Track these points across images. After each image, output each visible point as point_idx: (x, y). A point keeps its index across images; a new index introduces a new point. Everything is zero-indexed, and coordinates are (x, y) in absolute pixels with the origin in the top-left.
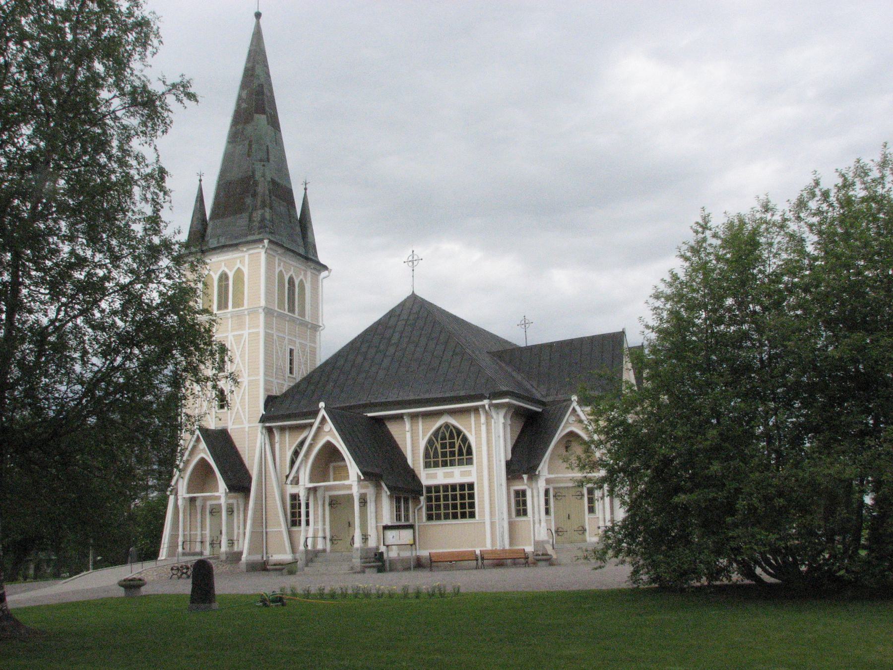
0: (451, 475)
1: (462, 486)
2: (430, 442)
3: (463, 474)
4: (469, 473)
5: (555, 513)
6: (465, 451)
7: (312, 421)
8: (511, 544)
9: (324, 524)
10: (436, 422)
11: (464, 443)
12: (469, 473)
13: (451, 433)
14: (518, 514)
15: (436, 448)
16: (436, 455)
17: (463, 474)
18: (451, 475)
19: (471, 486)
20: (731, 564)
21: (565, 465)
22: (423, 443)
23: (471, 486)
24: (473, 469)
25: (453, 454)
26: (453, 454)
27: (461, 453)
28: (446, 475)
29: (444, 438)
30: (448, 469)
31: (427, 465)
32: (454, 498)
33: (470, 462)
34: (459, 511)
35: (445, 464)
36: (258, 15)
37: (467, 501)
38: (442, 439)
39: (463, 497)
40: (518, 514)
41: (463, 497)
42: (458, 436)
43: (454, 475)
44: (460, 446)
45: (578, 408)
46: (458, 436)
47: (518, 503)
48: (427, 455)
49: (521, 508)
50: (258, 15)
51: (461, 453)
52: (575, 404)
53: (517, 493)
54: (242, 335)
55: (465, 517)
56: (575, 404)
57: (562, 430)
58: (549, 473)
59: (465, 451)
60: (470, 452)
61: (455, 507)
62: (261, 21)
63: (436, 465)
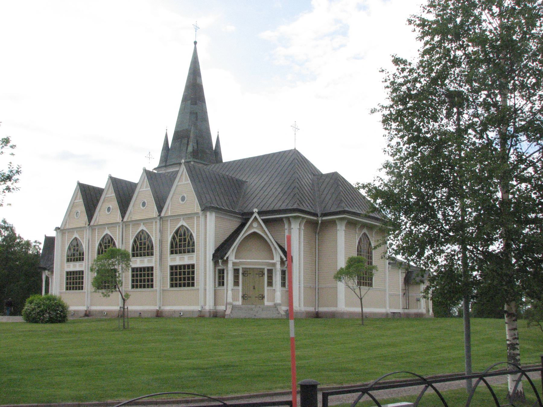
4: (81, 266)
5: (243, 283)
8: (215, 304)
10: (336, 247)
11: (191, 240)
14: (219, 285)
17: (180, 259)
20: (533, 36)
21: (70, 255)
28: (142, 261)
29: (181, 236)
30: (142, 258)
36: (195, 43)
40: (219, 285)
45: (258, 217)
48: (172, 247)
50: (195, 43)
52: (255, 215)
54: (255, 217)
56: (255, 215)
57: (246, 232)
58: (235, 259)
62: (197, 45)
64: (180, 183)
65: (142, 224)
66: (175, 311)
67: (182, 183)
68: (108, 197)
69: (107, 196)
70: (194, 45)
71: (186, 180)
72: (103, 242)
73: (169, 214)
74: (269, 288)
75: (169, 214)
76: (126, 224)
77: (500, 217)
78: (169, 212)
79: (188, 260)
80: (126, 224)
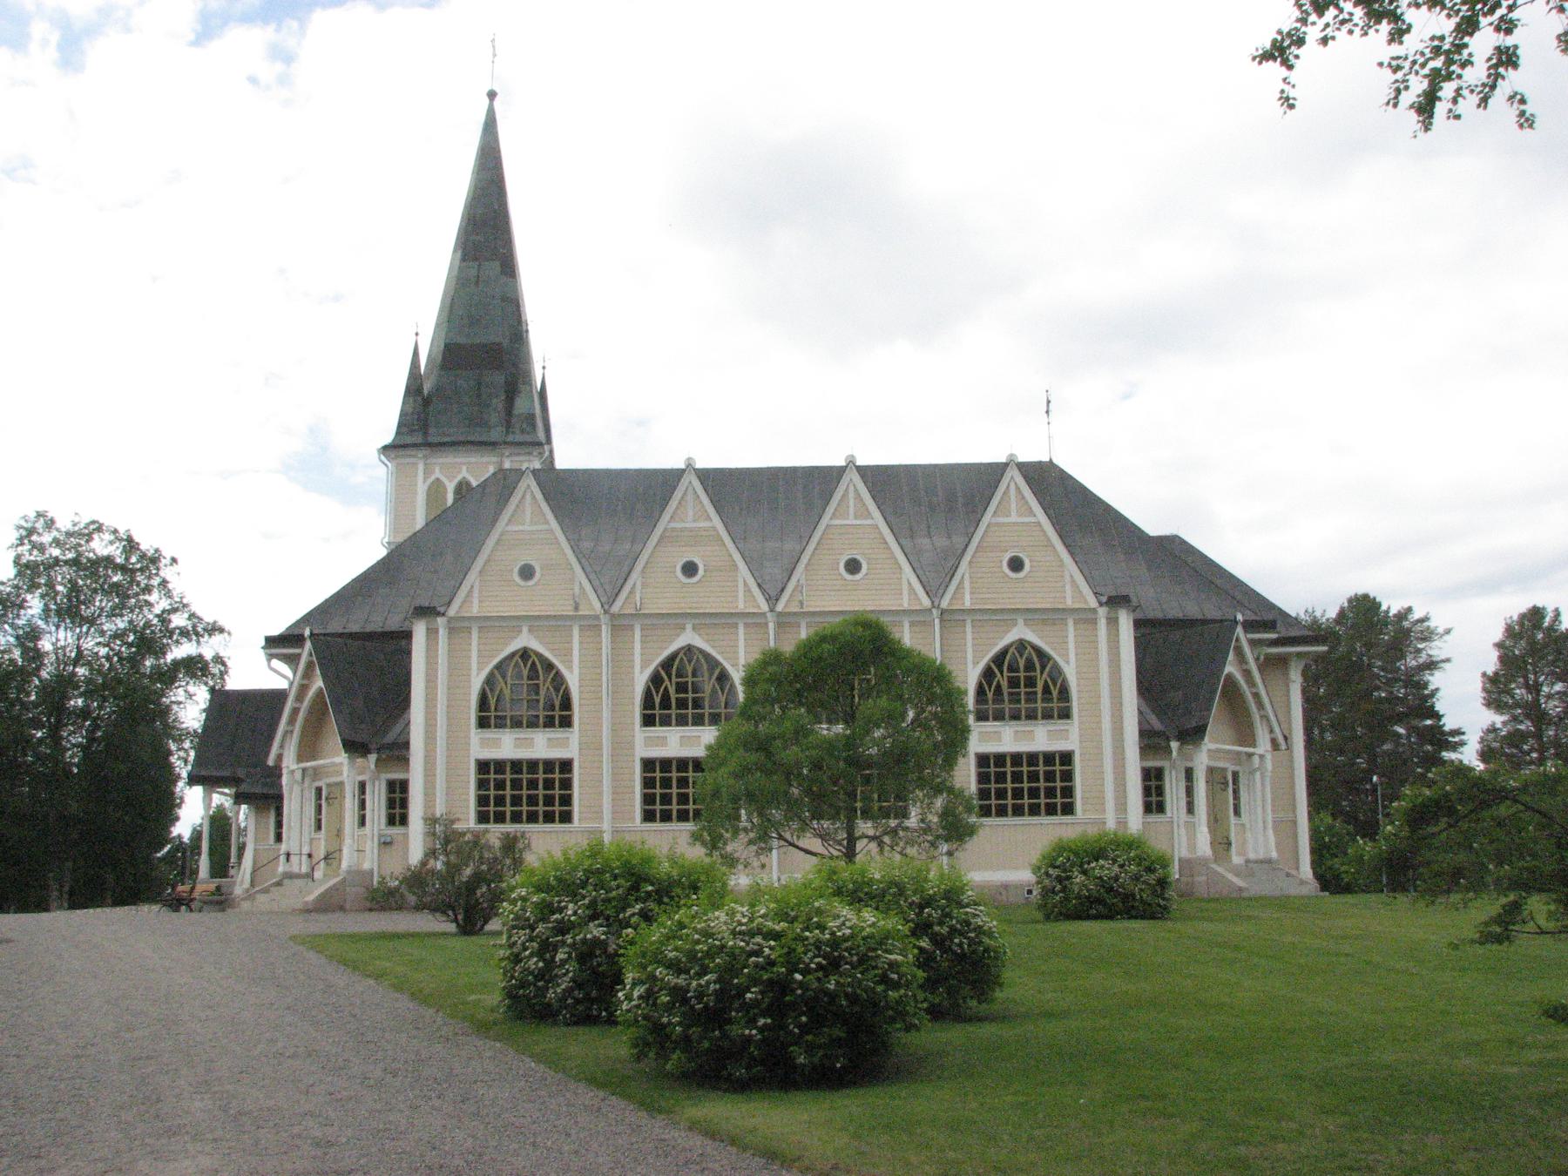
0: (663, 741)
2: (656, 680)
4: (564, 743)
7: (297, 651)
11: (557, 690)
12: (564, 743)
15: (999, 686)
16: (665, 703)
17: (519, 743)
18: (663, 741)
19: (1067, 758)
22: (641, 679)
23: (1067, 758)
32: (533, 784)
33: (1065, 714)
34: (1010, 802)
35: (682, 721)
36: (492, 95)
37: (1059, 784)
38: (1010, 669)
42: (711, 670)
44: (714, 691)
46: (1043, 668)
48: (648, 702)
50: (492, 95)
53: (391, 785)
55: (553, 821)
59: (657, 700)
62: (496, 103)
64: (509, 528)
65: (525, 629)
66: (1006, 886)
67: (1006, 520)
68: (673, 530)
69: (672, 525)
70: (487, 101)
71: (864, 513)
72: (1000, 667)
73: (968, 604)
74: (358, 832)
75: (475, 610)
76: (621, 626)
77: (849, 718)
78: (967, 596)
79: (516, 746)
80: (621, 626)
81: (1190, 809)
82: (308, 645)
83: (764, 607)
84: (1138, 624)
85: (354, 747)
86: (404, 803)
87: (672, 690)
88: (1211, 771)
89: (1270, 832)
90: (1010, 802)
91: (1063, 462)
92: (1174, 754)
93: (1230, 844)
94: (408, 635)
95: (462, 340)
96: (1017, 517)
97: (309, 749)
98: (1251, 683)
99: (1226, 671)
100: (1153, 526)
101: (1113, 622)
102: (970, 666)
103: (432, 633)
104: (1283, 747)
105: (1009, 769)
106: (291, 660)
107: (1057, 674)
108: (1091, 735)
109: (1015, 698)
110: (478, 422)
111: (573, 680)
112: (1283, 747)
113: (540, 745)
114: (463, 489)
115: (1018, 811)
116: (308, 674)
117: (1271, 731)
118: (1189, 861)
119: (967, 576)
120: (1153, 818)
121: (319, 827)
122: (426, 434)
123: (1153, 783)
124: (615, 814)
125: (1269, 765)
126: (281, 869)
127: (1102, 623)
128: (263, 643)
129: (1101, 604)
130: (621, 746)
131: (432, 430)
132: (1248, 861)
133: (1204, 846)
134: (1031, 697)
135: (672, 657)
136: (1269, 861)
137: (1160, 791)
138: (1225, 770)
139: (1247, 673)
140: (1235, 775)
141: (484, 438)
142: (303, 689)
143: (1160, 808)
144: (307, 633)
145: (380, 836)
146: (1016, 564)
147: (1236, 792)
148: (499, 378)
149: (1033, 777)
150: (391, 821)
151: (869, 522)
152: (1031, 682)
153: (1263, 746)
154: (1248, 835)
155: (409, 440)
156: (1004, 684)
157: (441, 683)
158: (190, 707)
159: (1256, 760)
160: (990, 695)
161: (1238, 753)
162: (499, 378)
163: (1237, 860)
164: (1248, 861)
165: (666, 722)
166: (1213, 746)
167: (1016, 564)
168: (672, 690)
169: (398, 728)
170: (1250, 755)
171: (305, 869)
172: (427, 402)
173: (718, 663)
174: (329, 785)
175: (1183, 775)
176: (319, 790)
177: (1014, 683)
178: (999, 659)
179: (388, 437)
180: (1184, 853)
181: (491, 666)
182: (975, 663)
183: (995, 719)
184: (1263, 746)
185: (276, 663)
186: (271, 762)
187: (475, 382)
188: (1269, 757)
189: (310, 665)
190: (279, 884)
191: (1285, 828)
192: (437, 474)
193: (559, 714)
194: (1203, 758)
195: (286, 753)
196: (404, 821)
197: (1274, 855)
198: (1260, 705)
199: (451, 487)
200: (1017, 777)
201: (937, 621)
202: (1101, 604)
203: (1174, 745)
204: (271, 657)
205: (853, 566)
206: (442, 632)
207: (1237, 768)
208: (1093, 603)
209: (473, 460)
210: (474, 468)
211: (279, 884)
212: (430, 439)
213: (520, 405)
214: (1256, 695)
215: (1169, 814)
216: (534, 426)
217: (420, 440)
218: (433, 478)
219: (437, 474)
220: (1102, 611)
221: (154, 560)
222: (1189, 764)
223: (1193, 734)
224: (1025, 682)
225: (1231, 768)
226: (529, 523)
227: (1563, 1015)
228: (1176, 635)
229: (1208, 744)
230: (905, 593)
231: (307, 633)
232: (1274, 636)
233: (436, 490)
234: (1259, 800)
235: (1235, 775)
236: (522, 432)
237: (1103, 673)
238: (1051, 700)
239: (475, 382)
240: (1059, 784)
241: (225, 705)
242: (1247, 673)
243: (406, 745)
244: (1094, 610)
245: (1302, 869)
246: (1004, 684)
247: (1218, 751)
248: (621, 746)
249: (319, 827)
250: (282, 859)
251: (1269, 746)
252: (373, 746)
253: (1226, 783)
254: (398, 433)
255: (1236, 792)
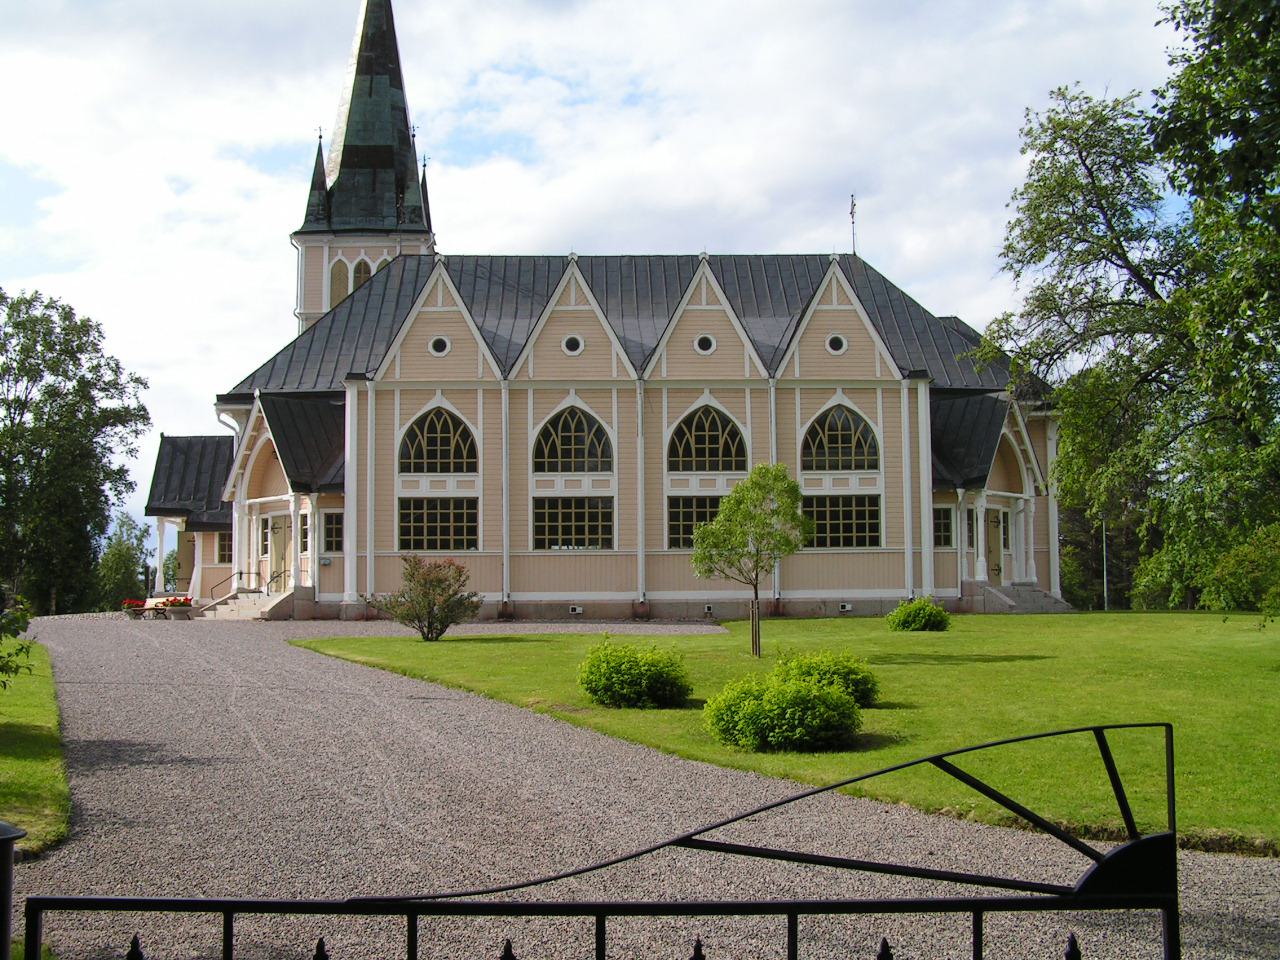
1: (459, 502)
3: (460, 484)
4: (873, 482)
6: (546, 452)
7: (248, 407)
9: (1027, 543)
12: (873, 482)
13: (713, 423)
15: (420, 444)
17: (460, 484)
19: (874, 500)
22: (533, 434)
24: (478, 478)
25: (579, 453)
26: (714, 453)
27: (727, 452)
29: (700, 427)
30: (841, 474)
31: (806, 466)
39: (861, 515)
41: (458, 518)
43: (852, 484)
44: (726, 442)
47: (329, 533)
48: (539, 452)
49: (334, 539)
51: (727, 452)
53: (329, 518)
59: (546, 452)
60: (607, 452)
61: (848, 528)
63: (419, 469)
78: (797, 369)
81: (971, 543)
82: (258, 403)
83: (634, 375)
84: (935, 393)
85: (301, 487)
86: (340, 533)
87: (558, 442)
88: (988, 511)
89: (1032, 562)
90: (828, 535)
91: (863, 255)
92: (960, 498)
93: (1000, 570)
94: (342, 395)
95: (358, 143)
96: (837, 302)
97: (259, 488)
98: (1021, 441)
99: (1002, 432)
100: (937, 311)
101: (913, 392)
102: (798, 426)
103: (362, 395)
104: (1045, 493)
105: (694, 509)
106: (242, 417)
107: (867, 431)
108: (894, 483)
109: (833, 452)
110: (372, 211)
111: (478, 434)
112: (1045, 493)
113: (451, 486)
114: (362, 268)
115: (835, 543)
116: (258, 427)
117: (1035, 481)
118: (970, 584)
119: (797, 354)
120: (942, 549)
121: (265, 551)
122: (329, 222)
123: (942, 520)
124: (648, 543)
125: (1033, 508)
126: (235, 585)
127: (905, 393)
128: (215, 401)
129: (904, 378)
130: (516, 487)
131: (335, 219)
132: (1013, 584)
133: (981, 575)
134: (847, 452)
135: (824, 415)
136: (1031, 585)
137: (948, 528)
138: (998, 511)
139: (1017, 434)
140: (1005, 515)
141: (379, 226)
142: (254, 440)
143: (948, 541)
144: (257, 393)
145: (320, 559)
146: (836, 344)
147: (1006, 532)
148: (390, 176)
149: (847, 515)
150: (329, 547)
151: (455, 308)
152: (846, 439)
153: (1028, 492)
154: (1014, 562)
155: (315, 227)
156: (825, 441)
157: (367, 439)
158: (135, 457)
159: (1021, 502)
160: (814, 450)
161: (1009, 498)
162: (390, 176)
163: (1005, 583)
164: (1013, 584)
165: (553, 468)
166: (990, 492)
167: (836, 344)
168: (558, 442)
169: (332, 471)
170: (1018, 499)
171: (253, 586)
172: (330, 194)
173: (863, 420)
174: (273, 518)
175: (965, 516)
176: (265, 522)
177: (833, 439)
178: (821, 420)
179: (298, 222)
180: (965, 577)
181: (546, 420)
182: (669, 424)
183: (844, 468)
184: (1028, 492)
185: (225, 417)
186: (225, 498)
187: (371, 182)
188: (1033, 500)
189: (260, 420)
190: (235, 597)
191: (1043, 557)
192: (340, 256)
193: (464, 458)
194: (981, 504)
195: (237, 492)
196: (339, 547)
197: (1034, 579)
198: (1027, 460)
199: (351, 268)
200: (835, 515)
201: (773, 389)
202: (904, 378)
203: (960, 491)
204: (219, 412)
205: (705, 344)
206: (371, 395)
207: (1006, 510)
208: (898, 376)
209: (369, 244)
210: (376, 253)
211: (235, 597)
212: (334, 227)
213: (410, 198)
214: (1024, 452)
215: (954, 547)
216: (421, 217)
217: (324, 227)
218: (336, 259)
219: (340, 256)
220: (905, 383)
221: (86, 327)
222: (971, 507)
223: (976, 483)
224: (838, 440)
225: (1003, 509)
226: (441, 300)
227: (4, 668)
228: (960, 402)
229: (986, 492)
230: (878, 365)
231: (257, 393)
232: (1039, 403)
233: (338, 272)
234: (1022, 533)
235: (1005, 515)
236: (412, 221)
237: (904, 430)
238: (863, 454)
239: (371, 182)
240: (600, 523)
241: (173, 450)
242: (1017, 434)
243: (341, 486)
244: (899, 382)
245: (1053, 590)
246: (825, 441)
247: (994, 496)
248: (516, 487)
249: (265, 551)
250: (235, 578)
251: (1033, 493)
252: (314, 487)
253: (997, 521)
254: (306, 222)
255: (1006, 532)
